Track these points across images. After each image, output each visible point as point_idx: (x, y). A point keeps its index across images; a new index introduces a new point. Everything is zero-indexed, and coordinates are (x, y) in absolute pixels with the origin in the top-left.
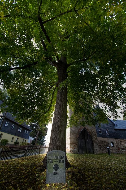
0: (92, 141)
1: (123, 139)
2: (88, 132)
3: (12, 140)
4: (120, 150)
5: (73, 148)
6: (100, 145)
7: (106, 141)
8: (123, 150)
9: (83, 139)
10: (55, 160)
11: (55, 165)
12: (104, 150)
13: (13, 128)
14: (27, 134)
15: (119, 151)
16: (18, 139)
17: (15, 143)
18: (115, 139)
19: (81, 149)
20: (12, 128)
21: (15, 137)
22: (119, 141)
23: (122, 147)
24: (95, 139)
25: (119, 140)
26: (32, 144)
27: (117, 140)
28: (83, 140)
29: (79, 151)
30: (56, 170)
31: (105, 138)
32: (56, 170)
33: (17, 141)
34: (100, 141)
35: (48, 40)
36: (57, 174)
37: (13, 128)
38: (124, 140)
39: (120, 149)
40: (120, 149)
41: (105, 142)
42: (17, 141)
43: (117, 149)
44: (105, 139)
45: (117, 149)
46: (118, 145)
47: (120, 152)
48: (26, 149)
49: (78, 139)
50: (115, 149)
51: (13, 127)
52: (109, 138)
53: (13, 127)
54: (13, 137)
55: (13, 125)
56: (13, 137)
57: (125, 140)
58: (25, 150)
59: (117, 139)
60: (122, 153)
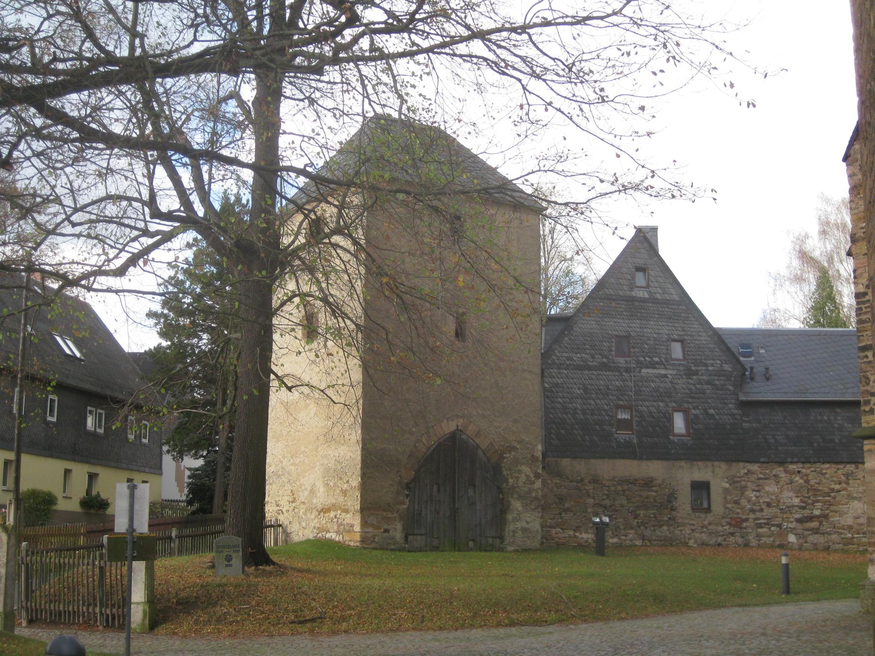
0: (500, 490)
1: (782, 463)
2: (478, 446)
3: (64, 492)
4: (744, 525)
5: (379, 528)
6: (608, 502)
7: (659, 482)
8: (760, 526)
9: (438, 485)
10: (227, 550)
11: (227, 556)
12: (632, 528)
13: (54, 419)
14: (145, 441)
15: (732, 534)
16: (92, 477)
17: (84, 503)
18: (723, 465)
19: (423, 532)
20: (49, 419)
21: (80, 472)
22: (753, 477)
23: (762, 510)
24: (523, 478)
25: (755, 467)
26: (190, 502)
27: (741, 469)
28: (439, 491)
29: (410, 538)
30: (229, 561)
31: (649, 463)
32: (229, 561)
33: (94, 493)
34: (607, 483)
35: (175, 77)
36: (231, 566)
37: (54, 419)
38: (786, 471)
39: (746, 520)
40: (746, 520)
41: (648, 483)
42: (94, 493)
43: (724, 522)
44: (654, 469)
45: (724, 522)
46: (736, 502)
47: (740, 540)
48: (171, 538)
49: (408, 487)
50: (710, 524)
51: (52, 415)
52: (683, 463)
53: (52, 415)
54: (67, 472)
55: (52, 401)
56: (67, 472)
57: (792, 467)
58: (168, 538)
59: (741, 464)
60: (754, 543)
